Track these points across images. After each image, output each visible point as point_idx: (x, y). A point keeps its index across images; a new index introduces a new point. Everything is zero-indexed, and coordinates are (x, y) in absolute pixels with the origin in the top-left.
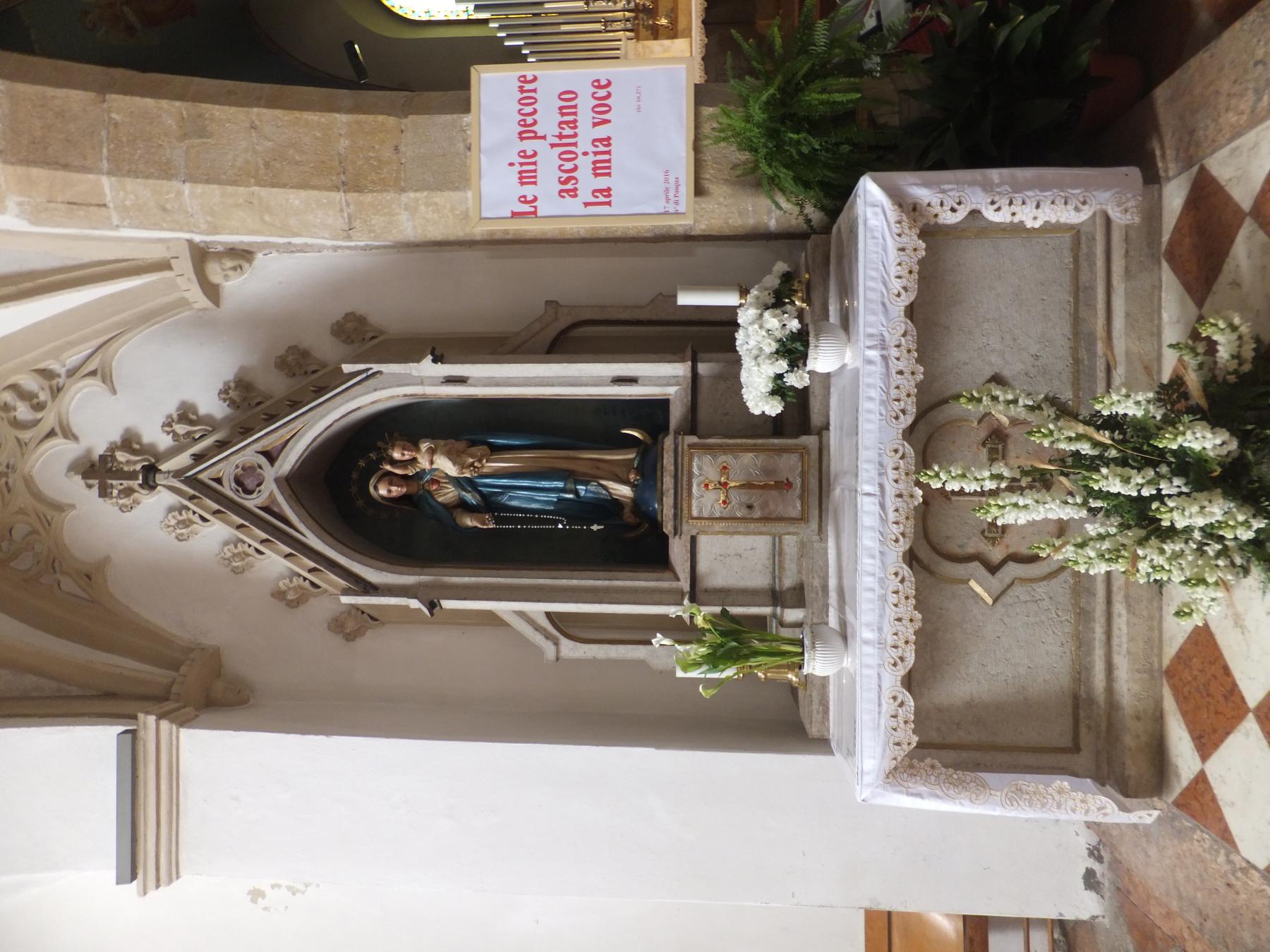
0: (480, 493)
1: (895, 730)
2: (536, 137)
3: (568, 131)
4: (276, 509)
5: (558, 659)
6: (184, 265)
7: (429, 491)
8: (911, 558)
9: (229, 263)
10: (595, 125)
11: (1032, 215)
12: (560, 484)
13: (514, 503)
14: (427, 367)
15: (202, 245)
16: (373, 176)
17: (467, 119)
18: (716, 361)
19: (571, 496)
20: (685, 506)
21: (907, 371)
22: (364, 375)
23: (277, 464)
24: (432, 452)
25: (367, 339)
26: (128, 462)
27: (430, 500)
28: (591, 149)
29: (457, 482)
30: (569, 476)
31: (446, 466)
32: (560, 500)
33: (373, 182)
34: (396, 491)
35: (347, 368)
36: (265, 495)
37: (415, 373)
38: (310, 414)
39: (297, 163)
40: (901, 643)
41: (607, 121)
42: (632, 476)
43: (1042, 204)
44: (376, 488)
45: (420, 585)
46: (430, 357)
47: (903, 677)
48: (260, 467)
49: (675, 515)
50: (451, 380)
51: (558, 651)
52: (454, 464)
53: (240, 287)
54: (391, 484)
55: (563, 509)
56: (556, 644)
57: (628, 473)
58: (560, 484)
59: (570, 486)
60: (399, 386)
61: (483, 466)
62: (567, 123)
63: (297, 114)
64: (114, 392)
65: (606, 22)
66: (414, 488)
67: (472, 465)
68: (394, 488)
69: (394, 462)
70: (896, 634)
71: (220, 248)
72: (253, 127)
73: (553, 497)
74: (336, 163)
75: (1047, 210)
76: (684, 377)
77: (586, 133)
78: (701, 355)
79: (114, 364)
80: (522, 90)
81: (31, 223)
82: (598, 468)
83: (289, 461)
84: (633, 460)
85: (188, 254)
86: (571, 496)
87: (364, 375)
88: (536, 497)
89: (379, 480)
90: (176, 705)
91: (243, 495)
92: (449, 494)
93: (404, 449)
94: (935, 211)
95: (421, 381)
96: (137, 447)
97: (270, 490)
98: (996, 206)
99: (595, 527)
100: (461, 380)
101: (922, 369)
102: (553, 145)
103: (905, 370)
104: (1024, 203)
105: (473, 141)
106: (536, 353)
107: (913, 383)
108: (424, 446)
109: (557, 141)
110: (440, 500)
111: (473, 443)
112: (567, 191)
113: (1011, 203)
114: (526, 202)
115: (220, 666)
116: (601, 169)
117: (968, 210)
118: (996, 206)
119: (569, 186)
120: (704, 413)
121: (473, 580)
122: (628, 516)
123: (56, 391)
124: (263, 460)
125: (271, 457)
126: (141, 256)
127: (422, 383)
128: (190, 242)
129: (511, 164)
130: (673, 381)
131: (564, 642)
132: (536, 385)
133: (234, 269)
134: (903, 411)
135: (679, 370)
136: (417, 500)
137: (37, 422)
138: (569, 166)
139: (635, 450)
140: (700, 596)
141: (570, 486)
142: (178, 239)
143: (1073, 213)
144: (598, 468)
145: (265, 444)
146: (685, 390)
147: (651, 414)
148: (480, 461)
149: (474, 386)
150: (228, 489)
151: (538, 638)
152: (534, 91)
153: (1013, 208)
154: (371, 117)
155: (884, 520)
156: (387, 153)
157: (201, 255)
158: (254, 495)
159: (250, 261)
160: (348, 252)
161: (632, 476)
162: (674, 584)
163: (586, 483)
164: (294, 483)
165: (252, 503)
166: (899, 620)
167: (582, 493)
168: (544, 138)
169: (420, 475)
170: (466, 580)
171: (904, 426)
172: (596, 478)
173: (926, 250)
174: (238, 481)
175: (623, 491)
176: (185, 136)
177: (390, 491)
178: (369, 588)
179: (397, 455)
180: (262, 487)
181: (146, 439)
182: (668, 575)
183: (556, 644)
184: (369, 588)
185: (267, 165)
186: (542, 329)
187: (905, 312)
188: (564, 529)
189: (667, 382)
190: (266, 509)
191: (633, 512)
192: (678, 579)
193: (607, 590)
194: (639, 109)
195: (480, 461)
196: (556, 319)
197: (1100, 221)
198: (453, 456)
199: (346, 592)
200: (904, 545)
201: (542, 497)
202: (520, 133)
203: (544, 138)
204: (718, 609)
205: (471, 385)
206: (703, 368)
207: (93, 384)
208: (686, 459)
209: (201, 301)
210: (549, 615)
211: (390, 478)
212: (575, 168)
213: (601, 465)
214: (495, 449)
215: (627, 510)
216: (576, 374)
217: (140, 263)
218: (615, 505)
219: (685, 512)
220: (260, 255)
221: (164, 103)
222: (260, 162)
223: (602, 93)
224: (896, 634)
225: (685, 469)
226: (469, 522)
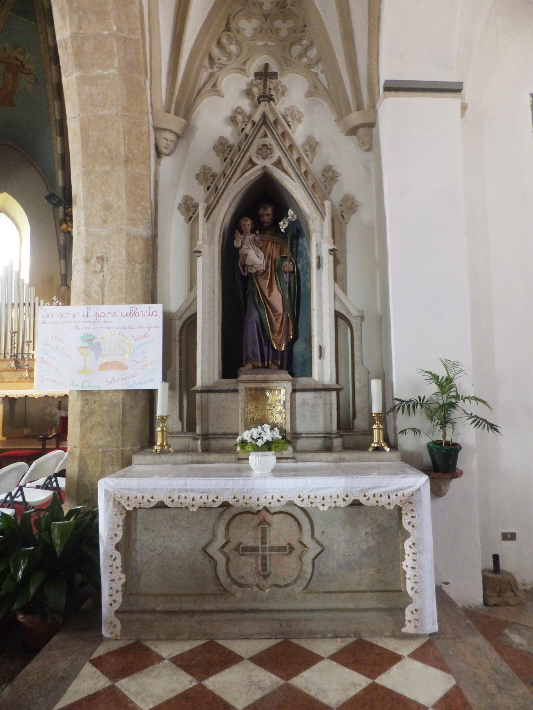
1: (331, 497)
8: (226, 505)
11: (408, 565)
21: (194, 503)
40: (310, 500)
43: (414, 570)
47: (358, 500)
70: (316, 497)
75: (411, 573)
83: (278, 175)
94: (409, 514)
98: (412, 546)
101: (326, 510)
103: (390, 499)
104: (414, 560)
107: (383, 504)
113: (414, 553)
117: (409, 531)
118: (412, 546)
125: (278, 164)
134: (173, 501)
143: (410, 586)
153: (411, 555)
155: (180, 490)
166: (323, 499)
171: (165, 501)
173: (324, 511)
187: (290, 501)
189: (322, 374)
197: (120, 616)
200: (232, 502)
210: (195, 315)
224: (316, 497)
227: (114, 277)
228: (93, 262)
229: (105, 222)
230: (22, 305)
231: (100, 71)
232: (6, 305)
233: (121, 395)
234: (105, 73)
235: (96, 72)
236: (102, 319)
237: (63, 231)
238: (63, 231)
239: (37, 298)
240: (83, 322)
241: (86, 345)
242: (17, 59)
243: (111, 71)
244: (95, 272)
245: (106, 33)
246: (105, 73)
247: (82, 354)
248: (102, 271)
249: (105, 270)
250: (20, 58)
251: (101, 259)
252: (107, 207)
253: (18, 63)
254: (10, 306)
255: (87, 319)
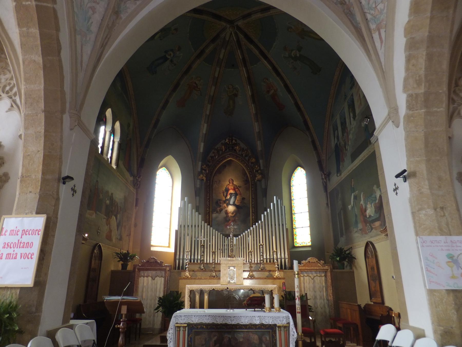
2: (22, 235)
3: (22, 245)
10: (21, 254)
16: (24, 185)
17: (34, 213)
28: (15, 253)
33: (23, 185)
39: (29, 164)
41: (21, 258)
62: (24, 245)
63: (42, 163)
64: (7, 112)
65: (215, 252)
72: (38, 151)
74: (29, 175)
77: (19, 251)
80: (36, 230)
81: (404, 117)
102: (19, 240)
105: (28, 216)
109: (20, 242)
112: (5, 245)
114: (5, 232)
116: (9, 256)
119: (6, 246)
123: (10, 97)
129: (16, 227)
137: (3, 92)
138: (12, 246)
152: (35, 234)
154: (40, 184)
156: (30, 189)
168: (21, 238)
176: (35, 133)
185: (29, 155)
194: (22, 268)
202: (24, 230)
203: (21, 238)
204: (296, 276)
207: (9, 105)
212: (11, 248)
221: (43, 127)
222: (29, 154)
223: (30, 256)
227: (452, 219)
228: (438, 210)
229: (440, 187)
230: (186, 226)
231: (436, 109)
232: (184, 226)
233: (18, 291)
234: (438, 110)
235: (434, 110)
236: (454, 245)
237: (199, 179)
238: (199, 179)
239: (203, 222)
240: (445, 246)
241: (450, 260)
242: (195, 83)
243: (441, 109)
244: (441, 216)
245: (441, 91)
246: (438, 110)
247: (449, 266)
248: (444, 216)
249: (447, 214)
250: (197, 82)
251: (442, 208)
252: (440, 179)
253: (195, 85)
254: (186, 226)
255: (446, 244)
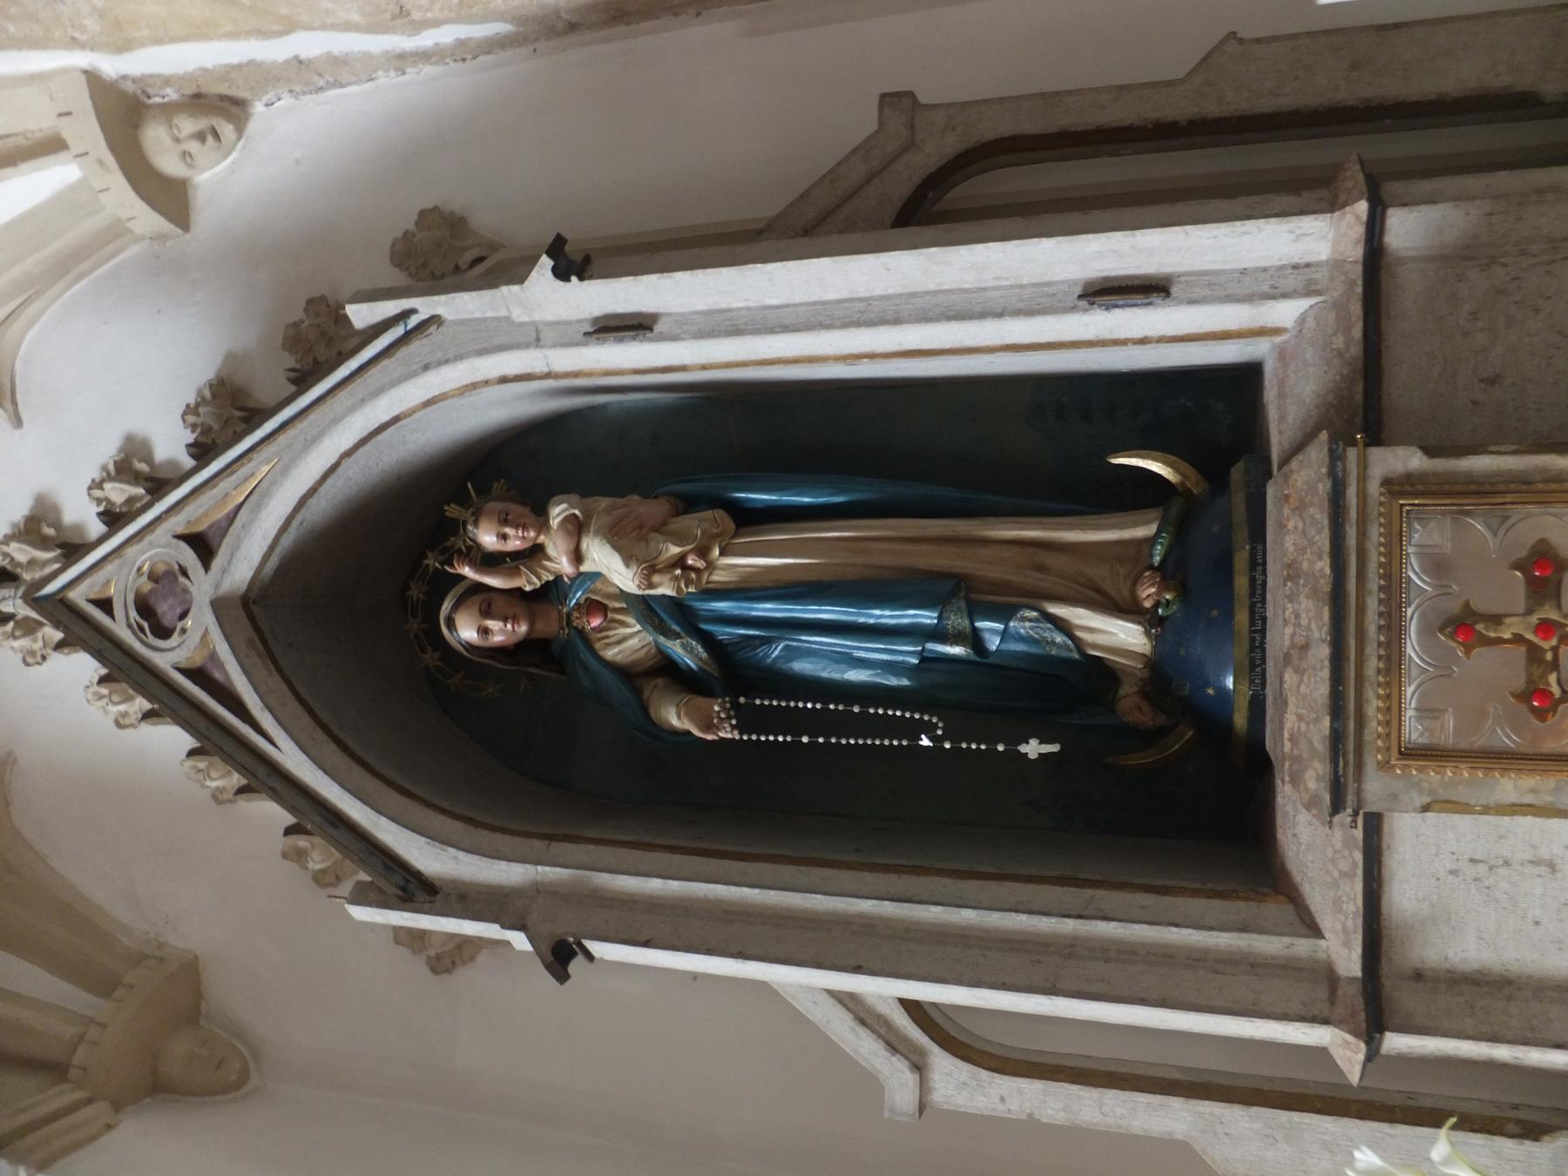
0: (708, 640)
4: (218, 675)
5: (922, 1107)
6: (87, 132)
7: (581, 633)
9: (187, 125)
12: (927, 617)
13: (802, 666)
14: (545, 296)
15: (129, 87)
18: (1457, 199)
19: (957, 650)
20: (1373, 706)
22: (397, 331)
23: (217, 563)
24: (577, 528)
25: (448, 252)
26: (32, 563)
27: (584, 654)
29: (645, 608)
30: (953, 594)
31: (608, 564)
32: (927, 660)
34: (501, 632)
35: (361, 315)
36: (194, 638)
37: (519, 315)
38: (282, 439)
42: (1147, 593)
44: (451, 623)
45: (538, 890)
46: (546, 262)
48: (184, 573)
49: (1337, 739)
50: (614, 327)
51: (924, 1087)
52: (627, 560)
53: (233, 179)
54: (487, 613)
55: (936, 689)
56: (919, 1067)
57: (1136, 581)
58: (927, 617)
59: (958, 621)
60: (481, 352)
61: (711, 566)
64: (18, 422)
66: (548, 626)
67: (680, 562)
68: (493, 624)
69: (491, 561)
71: (171, 94)
73: (907, 653)
76: (1337, 264)
78: (1391, 188)
79: (18, 366)
82: (1041, 568)
83: (245, 559)
84: (1151, 542)
85: (88, 103)
86: (957, 650)
87: (397, 331)
88: (861, 651)
89: (456, 606)
90: (80, 1095)
91: (151, 639)
92: (629, 641)
93: (505, 522)
95: (535, 337)
96: (50, 532)
97: (200, 636)
99: (1032, 748)
100: (636, 326)
106: (849, 227)
108: (558, 512)
110: (610, 654)
111: (690, 504)
115: (197, 994)
120: (1404, 382)
121: (675, 887)
122: (1130, 704)
124: (188, 556)
125: (203, 545)
126: (20, 128)
127: (537, 342)
128: (93, 79)
130: (1291, 282)
131: (943, 1065)
132: (846, 324)
133: (200, 137)
135: (1317, 239)
136: (552, 648)
139: (1154, 514)
140: (1401, 997)
141: (958, 621)
142: (65, 71)
144: (1041, 568)
145: (198, 515)
146: (1339, 306)
147: (1210, 411)
148: (703, 552)
149: (674, 338)
150: (121, 627)
151: (866, 1048)
157: (123, 113)
158: (174, 640)
159: (240, 123)
160: (428, 70)
161: (1147, 593)
162: (1302, 947)
163: (1004, 613)
164: (257, 613)
165: (168, 657)
167: (993, 643)
169: (553, 591)
170: (655, 885)
172: (1035, 597)
174: (144, 607)
175: (1120, 636)
177: (484, 631)
178: (414, 889)
179: (488, 539)
180: (189, 622)
181: (69, 517)
182: (1274, 909)
183: (919, 1067)
184: (414, 889)
186: (871, 177)
188: (937, 749)
190: (198, 675)
191: (1145, 695)
192: (1315, 931)
193: (1071, 949)
195: (703, 552)
196: (910, 146)
198: (625, 541)
199: (362, 896)
201: (874, 650)
205: (662, 338)
206: (1407, 229)
208: (1375, 534)
209: (146, 219)
211: (486, 602)
213: (1049, 559)
214: (749, 519)
215: (1127, 689)
216: (969, 280)
217: (21, 141)
218: (1093, 674)
219: (1374, 727)
220: (258, 108)
225: (1374, 559)
226: (674, 717)
